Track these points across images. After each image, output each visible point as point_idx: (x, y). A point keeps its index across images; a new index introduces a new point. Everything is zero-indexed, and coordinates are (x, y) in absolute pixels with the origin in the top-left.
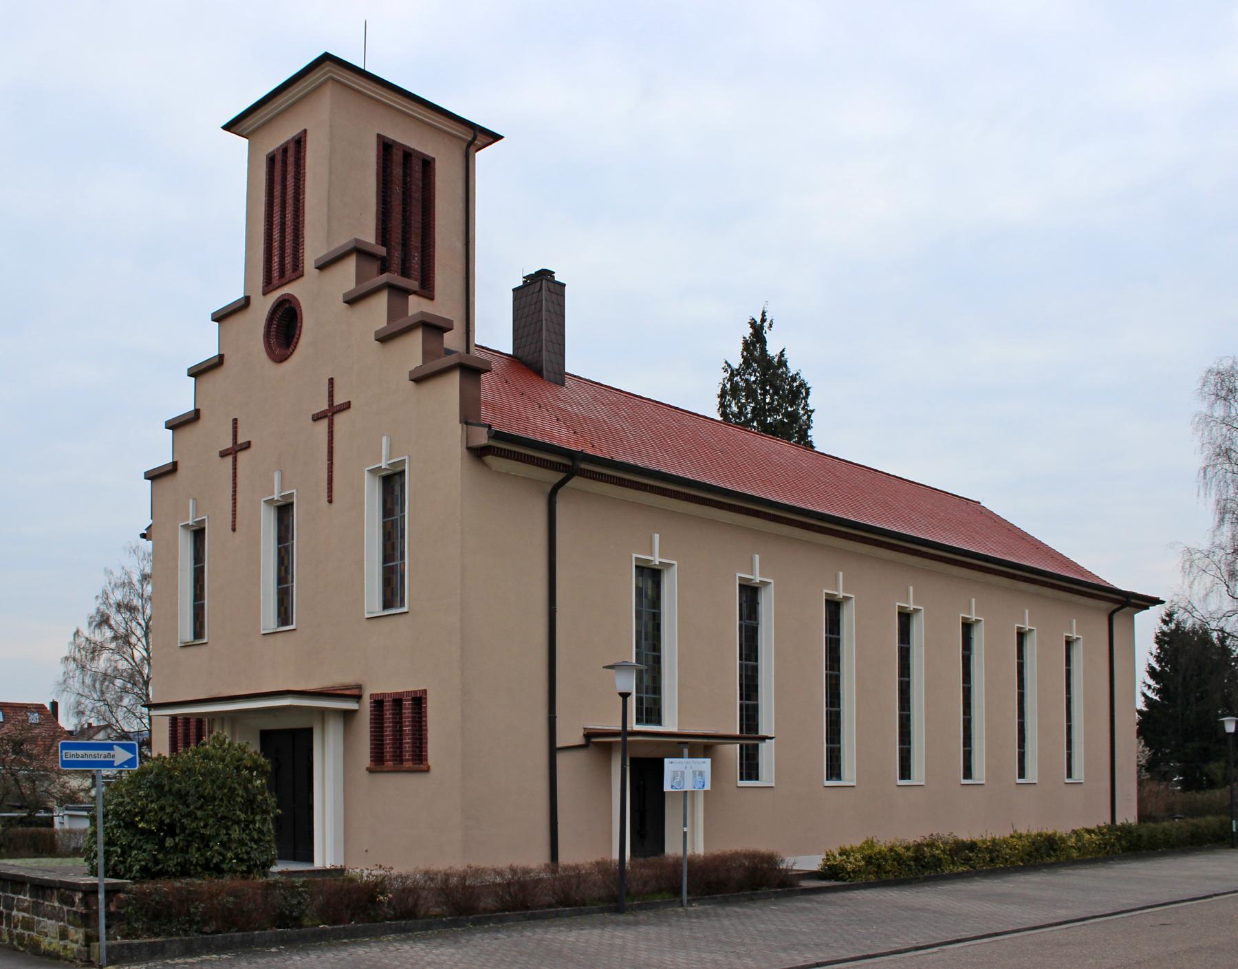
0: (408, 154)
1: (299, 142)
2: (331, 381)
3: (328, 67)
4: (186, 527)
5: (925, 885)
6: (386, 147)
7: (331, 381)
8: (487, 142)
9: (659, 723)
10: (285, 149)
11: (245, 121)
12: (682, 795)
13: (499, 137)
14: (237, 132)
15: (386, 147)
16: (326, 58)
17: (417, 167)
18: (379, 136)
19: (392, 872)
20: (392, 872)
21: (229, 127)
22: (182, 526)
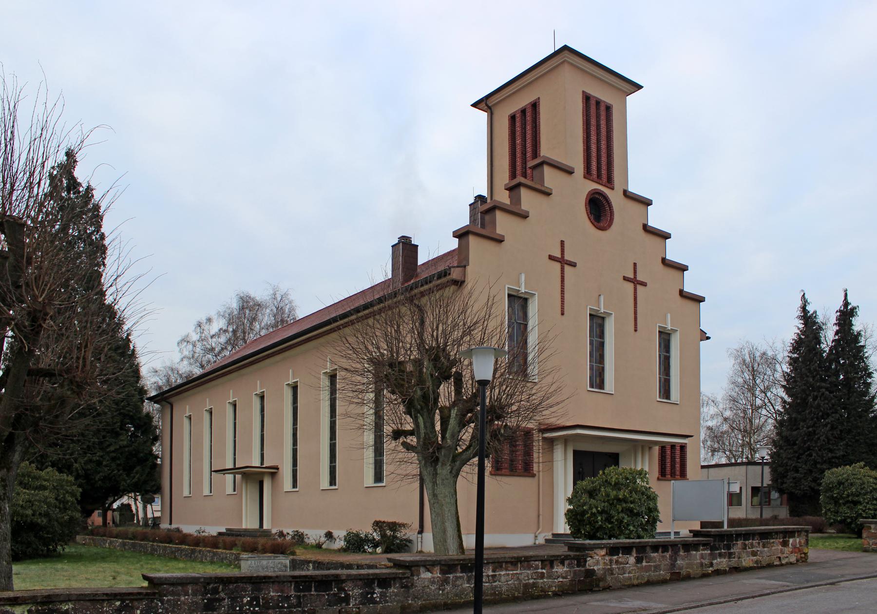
0: (598, 103)
1: (535, 106)
2: (635, 264)
3: (566, 53)
4: (288, 385)
5: (40, 562)
6: (587, 98)
7: (635, 264)
8: (633, 90)
9: (603, 389)
10: (523, 111)
11: (492, 97)
12: (511, 298)
13: (639, 87)
14: (480, 108)
15: (587, 98)
16: (565, 48)
17: (603, 108)
18: (583, 92)
19: (307, 539)
20: (307, 539)
21: (475, 105)
22: (323, 373)
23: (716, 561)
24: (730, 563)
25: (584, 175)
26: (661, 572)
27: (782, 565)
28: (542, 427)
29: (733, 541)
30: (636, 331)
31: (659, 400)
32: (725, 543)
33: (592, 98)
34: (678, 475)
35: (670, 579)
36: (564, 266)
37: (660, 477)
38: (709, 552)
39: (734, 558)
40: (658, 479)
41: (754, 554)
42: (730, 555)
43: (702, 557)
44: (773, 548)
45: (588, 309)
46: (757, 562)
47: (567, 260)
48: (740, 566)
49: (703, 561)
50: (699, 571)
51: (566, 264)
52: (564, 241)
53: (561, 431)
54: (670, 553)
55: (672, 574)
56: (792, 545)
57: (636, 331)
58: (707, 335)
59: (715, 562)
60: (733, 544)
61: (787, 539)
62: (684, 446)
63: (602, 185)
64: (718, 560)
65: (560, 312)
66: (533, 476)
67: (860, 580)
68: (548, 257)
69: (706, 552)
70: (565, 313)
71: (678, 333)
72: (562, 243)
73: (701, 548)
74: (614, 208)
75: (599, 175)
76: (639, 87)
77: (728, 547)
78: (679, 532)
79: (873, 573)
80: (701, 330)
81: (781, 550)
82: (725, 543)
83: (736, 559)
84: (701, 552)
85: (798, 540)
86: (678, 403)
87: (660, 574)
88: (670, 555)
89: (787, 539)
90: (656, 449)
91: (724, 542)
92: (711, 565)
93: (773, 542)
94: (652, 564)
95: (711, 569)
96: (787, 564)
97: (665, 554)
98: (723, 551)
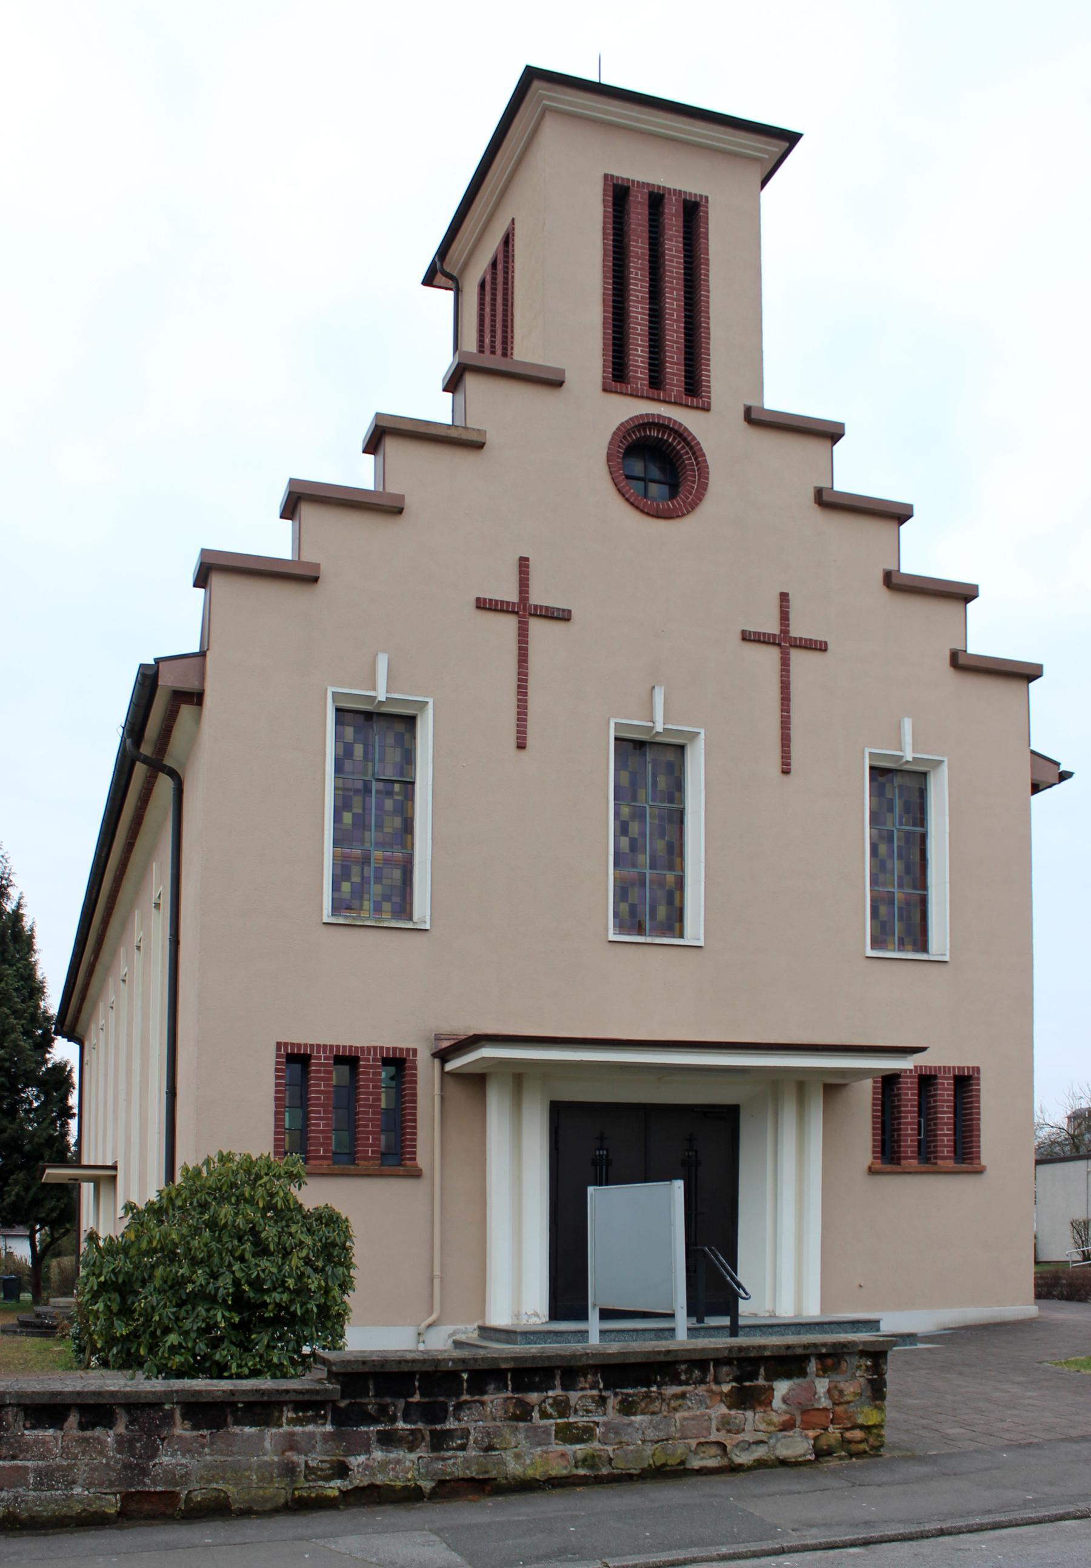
0: (656, 199)
7: (784, 597)
13: (791, 139)
23: (361, 1459)
24: (440, 1465)
25: (604, 384)
26: (78, 1490)
27: (735, 1469)
28: (445, 1044)
29: (459, 1394)
30: (786, 772)
31: (870, 953)
32: (417, 1398)
33: (634, 190)
34: (944, 1158)
35: (119, 1514)
36: (527, 623)
37: (879, 1165)
38: (329, 1428)
39: (463, 1448)
40: (871, 1171)
41: (569, 1434)
42: (439, 1441)
43: (291, 1444)
44: (678, 1415)
45: (612, 725)
46: (589, 1461)
47: (536, 607)
48: (493, 1474)
49: (299, 1459)
50: (278, 1490)
51: (535, 615)
52: (527, 559)
53: (459, 1056)
54: (121, 1428)
55: (127, 1497)
56: (785, 1400)
57: (786, 772)
58: (1062, 768)
59: (356, 1461)
60: (459, 1407)
61: (761, 1382)
62: (969, 1078)
63: (669, 403)
64: (378, 1455)
65: (513, 742)
66: (416, 1174)
67: (1031, 1528)
68: (473, 604)
69: (310, 1428)
70: (530, 742)
71: (945, 770)
72: (524, 564)
73: (291, 1415)
74: (708, 458)
75: (656, 380)
76: (791, 139)
77: (433, 1413)
78: (877, 1322)
79: (969, 1513)
80: (1033, 753)
81: (725, 1424)
82: (417, 1398)
83: (472, 1453)
84: (286, 1428)
85: (822, 1385)
86: (946, 959)
87: (69, 1497)
88: (120, 1440)
89: (761, 1382)
90: (865, 1093)
91: (412, 1395)
92: (342, 1470)
93: (683, 1396)
94: (29, 1464)
95: (338, 1483)
96: (761, 1464)
97: (98, 1432)
98: (400, 1425)
